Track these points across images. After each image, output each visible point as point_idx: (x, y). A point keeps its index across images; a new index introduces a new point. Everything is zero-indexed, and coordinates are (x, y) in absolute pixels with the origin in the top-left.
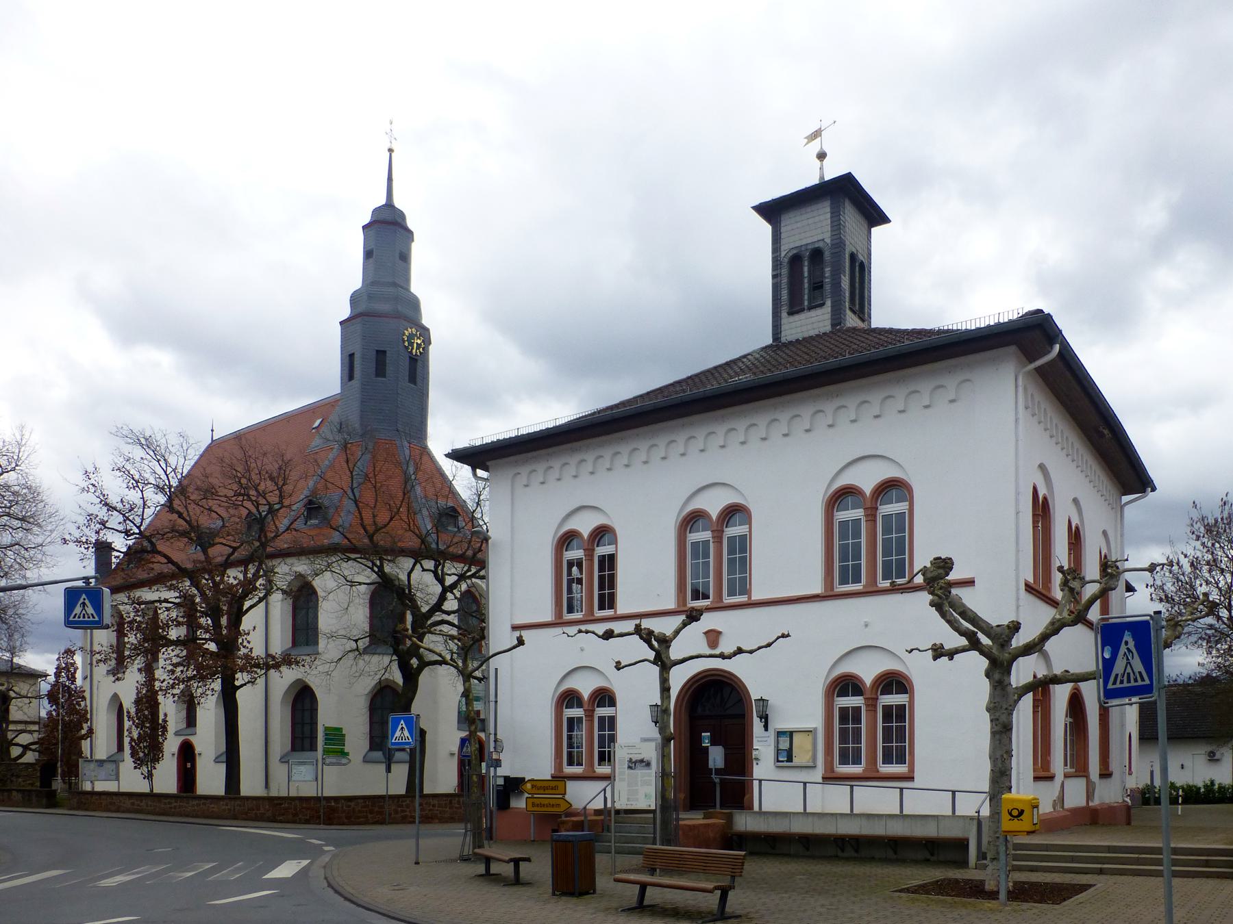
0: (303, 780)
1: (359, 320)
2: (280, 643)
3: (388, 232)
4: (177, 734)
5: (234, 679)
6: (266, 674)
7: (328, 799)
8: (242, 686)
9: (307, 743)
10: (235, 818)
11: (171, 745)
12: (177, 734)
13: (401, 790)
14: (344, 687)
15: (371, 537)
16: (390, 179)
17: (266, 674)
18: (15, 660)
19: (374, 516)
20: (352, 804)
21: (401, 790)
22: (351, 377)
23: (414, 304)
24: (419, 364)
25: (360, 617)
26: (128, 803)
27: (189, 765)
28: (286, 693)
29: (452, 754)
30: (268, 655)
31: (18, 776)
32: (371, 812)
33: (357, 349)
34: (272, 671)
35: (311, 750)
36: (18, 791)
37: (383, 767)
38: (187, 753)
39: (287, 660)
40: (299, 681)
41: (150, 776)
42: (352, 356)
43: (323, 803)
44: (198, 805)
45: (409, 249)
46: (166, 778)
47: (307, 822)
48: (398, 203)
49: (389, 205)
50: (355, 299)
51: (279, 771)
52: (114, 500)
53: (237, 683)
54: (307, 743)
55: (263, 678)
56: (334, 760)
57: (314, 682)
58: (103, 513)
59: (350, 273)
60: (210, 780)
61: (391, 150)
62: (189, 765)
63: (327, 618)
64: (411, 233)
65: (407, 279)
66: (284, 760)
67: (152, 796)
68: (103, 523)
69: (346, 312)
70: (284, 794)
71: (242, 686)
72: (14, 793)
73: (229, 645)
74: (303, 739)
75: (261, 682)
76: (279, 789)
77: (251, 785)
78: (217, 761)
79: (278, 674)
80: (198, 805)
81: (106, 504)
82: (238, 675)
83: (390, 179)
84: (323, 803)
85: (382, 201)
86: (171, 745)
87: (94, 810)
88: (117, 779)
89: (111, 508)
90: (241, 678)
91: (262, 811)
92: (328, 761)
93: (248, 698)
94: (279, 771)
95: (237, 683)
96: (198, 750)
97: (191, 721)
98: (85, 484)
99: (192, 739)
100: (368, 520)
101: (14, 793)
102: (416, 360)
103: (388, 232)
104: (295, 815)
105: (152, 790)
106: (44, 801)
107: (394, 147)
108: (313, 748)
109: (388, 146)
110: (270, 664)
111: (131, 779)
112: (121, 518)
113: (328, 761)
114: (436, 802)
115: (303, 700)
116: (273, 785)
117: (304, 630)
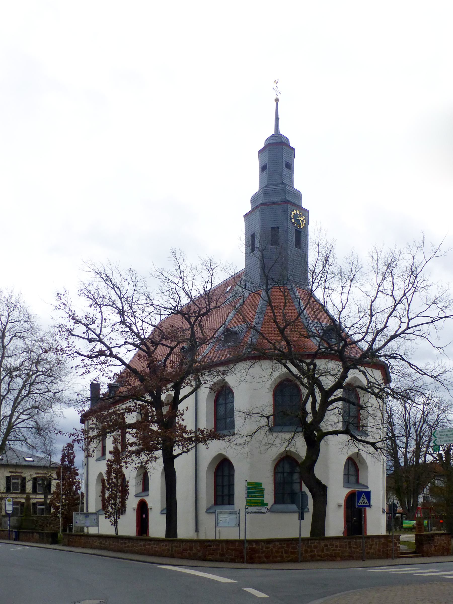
0: (226, 527)
1: (259, 209)
2: (206, 423)
3: (277, 156)
4: (136, 496)
5: (172, 450)
6: (196, 446)
7: (250, 542)
8: (178, 455)
9: (226, 499)
10: (172, 556)
11: (132, 503)
12: (136, 496)
13: (306, 533)
14: (253, 455)
15: (282, 331)
16: (277, 119)
17: (196, 446)
18: (52, 460)
19: (284, 315)
20: (270, 546)
21: (306, 533)
22: (253, 249)
23: (298, 195)
24: (302, 235)
25: (265, 402)
26: (97, 542)
27: (144, 516)
28: (211, 463)
29: (340, 506)
30: (197, 429)
31: (51, 524)
32: (286, 552)
33: (257, 230)
34: (201, 445)
35: (229, 504)
36: (37, 533)
37: (296, 516)
38: (143, 508)
39: (214, 435)
40: (220, 455)
41: (115, 524)
42: (253, 237)
43: (246, 545)
44: (145, 545)
45: (293, 161)
46: (128, 526)
47: (232, 561)
48: (282, 131)
49: (277, 134)
50: (254, 199)
51: (207, 521)
52: (80, 315)
53: (175, 453)
54: (226, 499)
55: (194, 450)
56: (255, 510)
57: (232, 454)
58: (70, 324)
59: (249, 182)
60: (157, 527)
61: (277, 100)
62: (144, 516)
63: (241, 402)
64: (293, 149)
65: (292, 181)
66: (209, 511)
67: (117, 538)
68: (70, 333)
69: (249, 208)
70: (211, 536)
71: (178, 455)
72: (35, 534)
73: (169, 423)
74: (223, 496)
75: (192, 452)
76: (208, 533)
77: (185, 531)
78: (161, 513)
79: (205, 446)
80: (149, 545)
81: (73, 318)
82: (176, 447)
83: (277, 119)
84: (246, 545)
85: (272, 132)
86: (132, 503)
87: (77, 547)
88: (98, 525)
89: (77, 322)
90: (177, 450)
91: (194, 551)
92: (250, 510)
93: (183, 464)
94: (207, 521)
95: (175, 453)
96: (150, 505)
97: (146, 488)
98: (57, 304)
99: (147, 499)
100: (279, 318)
101: (35, 534)
102: (300, 232)
103: (277, 156)
104: (222, 555)
105: (117, 533)
106: (50, 539)
107: (279, 97)
108: (231, 502)
109: (275, 97)
110: (200, 438)
111: (105, 527)
112: (84, 329)
113: (250, 510)
114: (338, 543)
115: (223, 468)
116: (201, 529)
117: (223, 424)
